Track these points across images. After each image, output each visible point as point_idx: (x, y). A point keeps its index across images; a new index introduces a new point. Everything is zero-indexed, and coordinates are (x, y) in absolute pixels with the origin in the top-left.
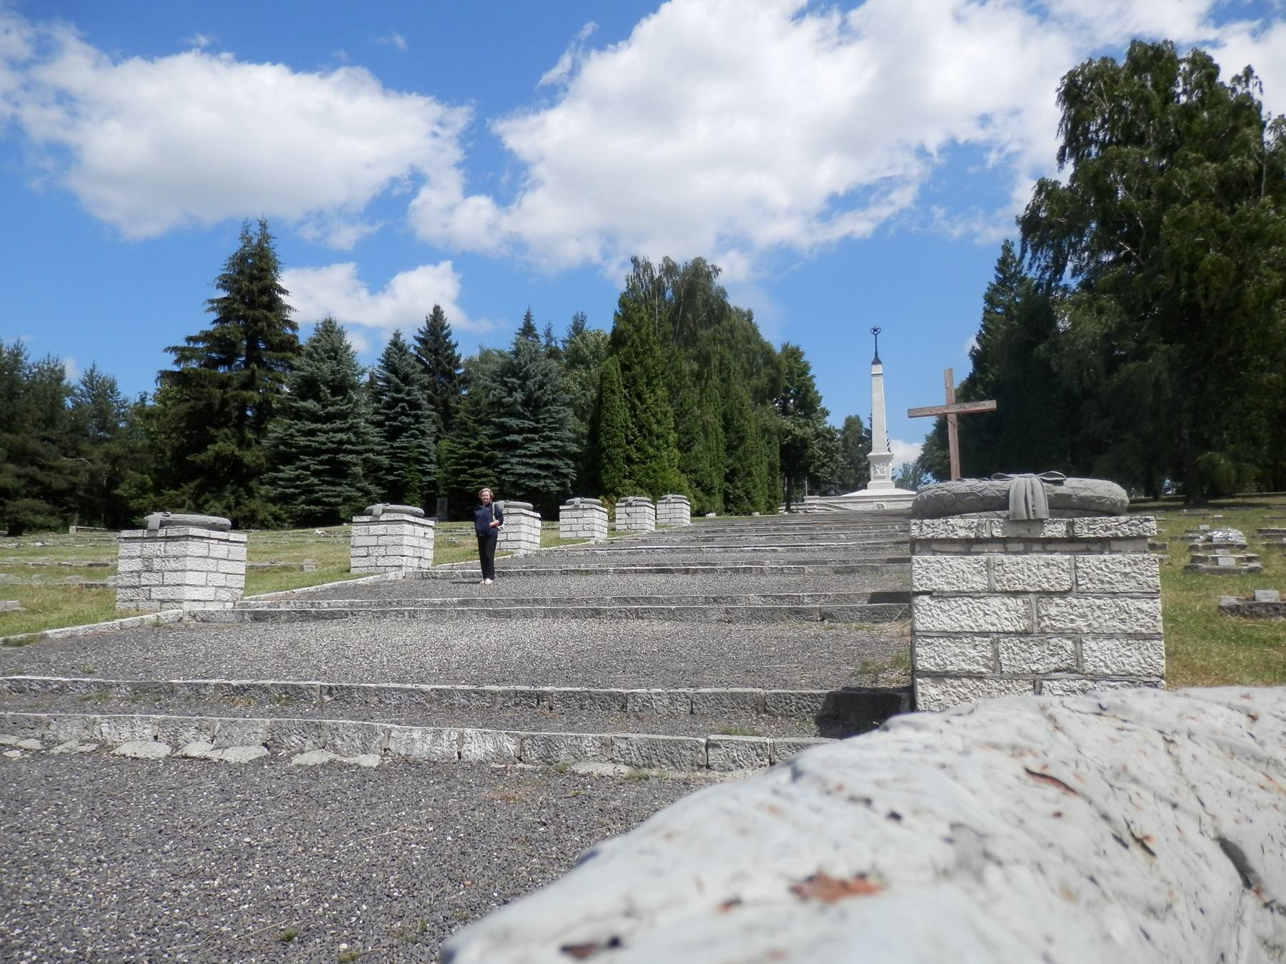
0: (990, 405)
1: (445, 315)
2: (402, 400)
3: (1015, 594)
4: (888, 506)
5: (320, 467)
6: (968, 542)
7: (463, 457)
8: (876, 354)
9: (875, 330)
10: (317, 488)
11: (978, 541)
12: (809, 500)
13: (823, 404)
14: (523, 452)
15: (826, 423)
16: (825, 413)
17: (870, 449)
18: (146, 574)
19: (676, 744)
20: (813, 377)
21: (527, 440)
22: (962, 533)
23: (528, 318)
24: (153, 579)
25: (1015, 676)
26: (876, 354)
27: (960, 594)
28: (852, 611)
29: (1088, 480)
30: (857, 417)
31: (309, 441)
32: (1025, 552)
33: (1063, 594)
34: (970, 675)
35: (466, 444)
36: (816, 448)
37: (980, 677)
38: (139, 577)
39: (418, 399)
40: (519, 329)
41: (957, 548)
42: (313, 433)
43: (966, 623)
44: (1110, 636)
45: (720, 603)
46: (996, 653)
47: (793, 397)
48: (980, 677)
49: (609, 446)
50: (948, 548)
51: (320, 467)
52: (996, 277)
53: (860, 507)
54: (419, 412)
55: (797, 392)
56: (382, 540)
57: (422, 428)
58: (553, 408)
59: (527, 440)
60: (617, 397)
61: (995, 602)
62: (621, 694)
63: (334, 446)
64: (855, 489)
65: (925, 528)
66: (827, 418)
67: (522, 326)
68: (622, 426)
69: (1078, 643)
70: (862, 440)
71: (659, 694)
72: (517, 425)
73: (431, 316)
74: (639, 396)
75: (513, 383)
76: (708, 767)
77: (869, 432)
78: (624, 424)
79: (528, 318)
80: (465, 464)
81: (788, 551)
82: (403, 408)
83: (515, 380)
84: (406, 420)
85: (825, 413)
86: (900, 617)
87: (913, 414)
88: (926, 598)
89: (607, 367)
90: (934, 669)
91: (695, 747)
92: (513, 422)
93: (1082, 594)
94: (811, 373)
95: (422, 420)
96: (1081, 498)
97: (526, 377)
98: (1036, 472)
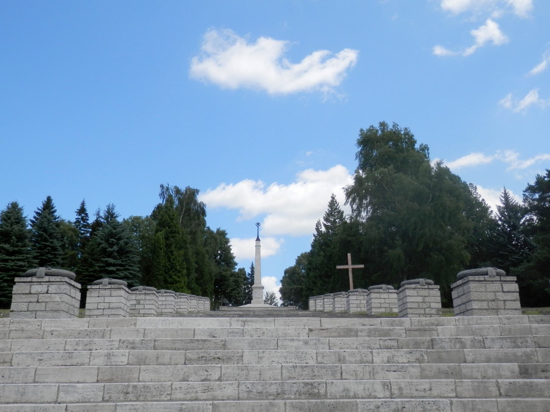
1: (53, 202)
2: (48, 246)
3: (421, 296)
5: (8, 278)
6: (414, 288)
7: (85, 276)
10: (5, 288)
11: (416, 288)
14: (116, 276)
18: (138, 305)
21: (118, 270)
22: (413, 287)
23: (83, 204)
24: (140, 307)
25: (422, 308)
27: (413, 296)
31: (4, 264)
33: (428, 296)
34: (415, 308)
35: (87, 270)
37: (417, 308)
38: (135, 306)
39: (57, 246)
40: (77, 210)
42: (6, 261)
43: (415, 301)
44: (434, 302)
46: (419, 305)
48: (417, 308)
49: (157, 274)
51: (8, 278)
52: (328, 210)
54: (57, 253)
56: (164, 303)
57: (58, 261)
58: (131, 256)
59: (118, 270)
60: (162, 251)
61: (418, 297)
63: (17, 268)
64: (246, 303)
67: (79, 208)
68: (164, 265)
69: (430, 303)
72: (114, 262)
73: (45, 201)
74: (171, 252)
75: (113, 241)
78: (165, 265)
79: (83, 204)
80: (86, 280)
82: (48, 250)
83: (113, 240)
84: (50, 256)
87: (252, 268)
89: (158, 237)
92: (111, 260)
93: (430, 296)
95: (57, 256)
97: (120, 239)
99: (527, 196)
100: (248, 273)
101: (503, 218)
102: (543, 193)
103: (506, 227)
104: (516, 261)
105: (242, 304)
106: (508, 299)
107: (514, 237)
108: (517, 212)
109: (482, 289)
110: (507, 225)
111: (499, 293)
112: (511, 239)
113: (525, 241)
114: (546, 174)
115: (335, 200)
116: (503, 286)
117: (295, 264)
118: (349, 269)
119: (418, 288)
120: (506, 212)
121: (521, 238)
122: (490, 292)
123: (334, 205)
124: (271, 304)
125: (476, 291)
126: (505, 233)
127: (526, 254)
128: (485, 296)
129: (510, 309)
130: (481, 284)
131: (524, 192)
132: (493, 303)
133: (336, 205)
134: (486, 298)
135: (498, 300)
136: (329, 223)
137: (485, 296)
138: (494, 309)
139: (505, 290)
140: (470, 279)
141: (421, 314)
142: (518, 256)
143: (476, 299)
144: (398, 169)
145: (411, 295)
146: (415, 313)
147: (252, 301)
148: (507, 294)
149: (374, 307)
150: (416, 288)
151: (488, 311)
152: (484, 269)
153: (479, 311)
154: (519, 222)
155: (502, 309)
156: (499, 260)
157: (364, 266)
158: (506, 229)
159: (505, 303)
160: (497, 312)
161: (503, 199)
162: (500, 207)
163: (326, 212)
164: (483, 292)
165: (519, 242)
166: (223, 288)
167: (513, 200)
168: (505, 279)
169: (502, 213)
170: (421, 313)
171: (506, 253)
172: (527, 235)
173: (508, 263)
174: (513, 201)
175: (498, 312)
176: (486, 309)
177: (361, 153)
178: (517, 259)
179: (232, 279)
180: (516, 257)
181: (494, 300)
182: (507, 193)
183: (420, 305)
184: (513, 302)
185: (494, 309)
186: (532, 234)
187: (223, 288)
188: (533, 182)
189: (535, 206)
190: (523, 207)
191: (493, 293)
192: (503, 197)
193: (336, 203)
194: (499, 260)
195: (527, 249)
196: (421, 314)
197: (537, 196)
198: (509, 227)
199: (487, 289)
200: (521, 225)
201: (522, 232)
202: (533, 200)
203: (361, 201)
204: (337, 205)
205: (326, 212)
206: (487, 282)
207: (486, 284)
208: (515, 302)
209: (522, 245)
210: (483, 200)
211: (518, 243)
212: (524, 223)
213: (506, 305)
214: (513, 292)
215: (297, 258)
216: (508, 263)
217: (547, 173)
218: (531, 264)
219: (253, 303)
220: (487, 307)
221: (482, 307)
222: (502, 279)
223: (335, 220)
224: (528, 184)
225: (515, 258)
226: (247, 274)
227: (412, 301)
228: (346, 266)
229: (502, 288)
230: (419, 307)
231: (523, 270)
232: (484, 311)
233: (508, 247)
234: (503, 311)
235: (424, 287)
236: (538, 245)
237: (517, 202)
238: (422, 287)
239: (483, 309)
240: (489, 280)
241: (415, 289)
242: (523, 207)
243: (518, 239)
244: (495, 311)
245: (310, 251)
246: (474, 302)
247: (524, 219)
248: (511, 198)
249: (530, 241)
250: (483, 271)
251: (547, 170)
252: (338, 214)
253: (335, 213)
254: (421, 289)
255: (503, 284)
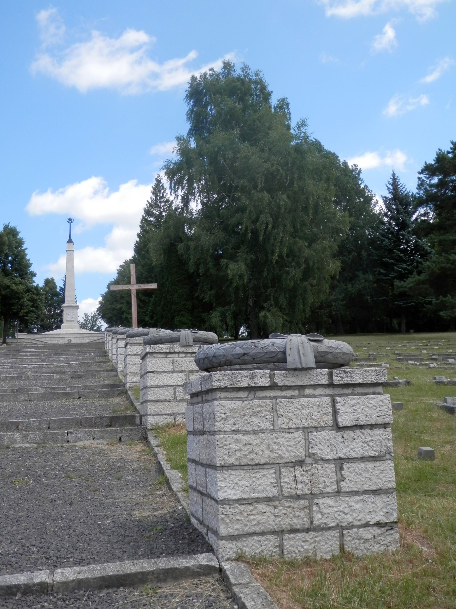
0: (154, 286)
3: (181, 372)
4: (74, 341)
6: (166, 353)
8: (70, 236)
9: (70, 220)
11: (170, 353)
12: (19, 336)
13: (32, 269)
15: (34, 282)
16: (34, 275)
17: (64, 302)
19: (55, 434)
20: (26, 249)
22: (164, 350)
25: (181, 400)
26: (70, 236)
27: (162, 372)
28: (94, 393)
29: (206, 332)
30: (52, 278)
32: (185, 357)
34: (166, 401)
36: (26, 298)
37: (169, 401)
41: (163, 356)
43: (165, 383)
45: (20, 392)
46: (175, 393)
47: (10, 262)
48: (169, 401)
50: (159, 355)
52: (151, 198)
53: (55, 342)
55: (14, 260)
61: (175, 375)
62: (16, 422)
65: (151, 348)
66: (34, 279)
70: (57, 294)
71: (34, 421)
76: (68, 441)
77: (63, 290)
81: (33, 368)
85: (34, 275)
86: (118, 395)
88: (151, 374)
90: (153, 399)
91: (63, 434)
94: (24, 247)
96: (203, 338)
98: (189, 329)
99: (423, 180)
100: (60, 287)
101: (389, 213)
102: (445, 177)
103: (393, 226)
104: (403, 272)
105: (51, 329)
106: (354, 455)
107: (403, 239)
108: (407, 205)
109: (258, 423)
110: (394, 223)
111: (323, 433)
112: (398, 242)
113: (416, 245)
114: (451, 148)
115: (161, 185)
116: (338, 406)
117: (117, 275)
118: (132, 291)
119: (175, 353)
120: (395, 205)
121: (412, 241)
122: (288, 430)
123: (160, 191)
124: (92, 329)
125: (235, 432)
126: (392, 233)
127: (418, 262)
128: (268, 446)
129: (357, 493)
130: (256, 402)
131: (420, 173)
132: (298, 472)
133: (162, 191)
134: (272, 455)
135: (316, 462)
136: (152, 217)
137: (268, 446)
138: (298, 497)
139: (343, 421)
140: (215, 384)
141: (179, 414)
142: (407, 265)
143: (232, 460)
144: (244, 138)
145: (159, 370)
146: (164, 412)
147: (62, 326)
148: (349, 434)
149: (131, 373)
150: (170, 353)
151: (275, 507)
152: (275, 341)
153: (242, 508)
154: (411, 218)
155: (328, 495)
156: (382, 271)
157: (158, 286)
158: (394, 228)
159: (341, 469)
160: (310, 507)
161: (391, 187)
162: (386, 197)
163: (148, 201)
164: (261, 431)
165: (409, 246)
166: (15, 309)
167: (404, 188)
168: (347, 380)
169: (388, 207)
170: (179, 412)
171: (392, 261)
172: (419, 237)
173: (393, 274)
174: (404, 190)
175: (315, 508)
176: (268, 500)
177: (192, 111)
178: (405, 269)
179: (26, 297)
180: (404, 266)
181: (301, 463)
182: (396, 179)
183: (177, 394)
184: (370, 465)
185: (298, 497)
186: (426, 236)
187: (15, 309)
188: (432, 161)
189: (432, 194)
190: (417, 195)
191: (299, 435)
192: (390, 184)
193: (163, 188)
194: (382, 271)
195: (418, 255)
196: (179, 414)
197: (435, 180)
198: (396, 225)
199: (280, 421)
200: (413, 223)
201: (414, 232)
202: (431, 186)
203: (190, 182)
204: (164, 192)
205: (148, 201)
206: (279, 393)
207: (275, 398)
208: (378, 463)
209: (412, 250)
210: (366, 187)
211: (407, 248)
212: (416, 219)
213: (343, 479)
214: (372, 426)
215: (119, 268)
216: (393, 274)
217: (452, 146)
218: (423, 277)
219: (63, 329)
220: (274, 492)
221: (254, 491)
222: (336, 380)
223: (161, 213)
224: (426, 162)
225: (402, 268)
226: (58, 288)
227: (160, 384)
228: (127, 286)
229: (335, 412)
230: (175, 398)
231: (411, 285)
232: (262, 507)
233: (394, 253)
234: (329, 501)
235: (190, 350)
236: (432, 250)
237: (408, 190)
238: (185, 350)
239: (258, 500)
240: (288, 384)
241: (169, 356)
242: (417, 195)
243: (408, 242)
244: (303, 502)
245: (133, 257)
246: (226, 474)
247: (417, 213)
248: (401, 185)
249: (423, 245)
250: (271, 349)
251: (452, 143)
252: (165, 205)
253: (160, 202)
254: (183, 355)
255: (338, 399)
